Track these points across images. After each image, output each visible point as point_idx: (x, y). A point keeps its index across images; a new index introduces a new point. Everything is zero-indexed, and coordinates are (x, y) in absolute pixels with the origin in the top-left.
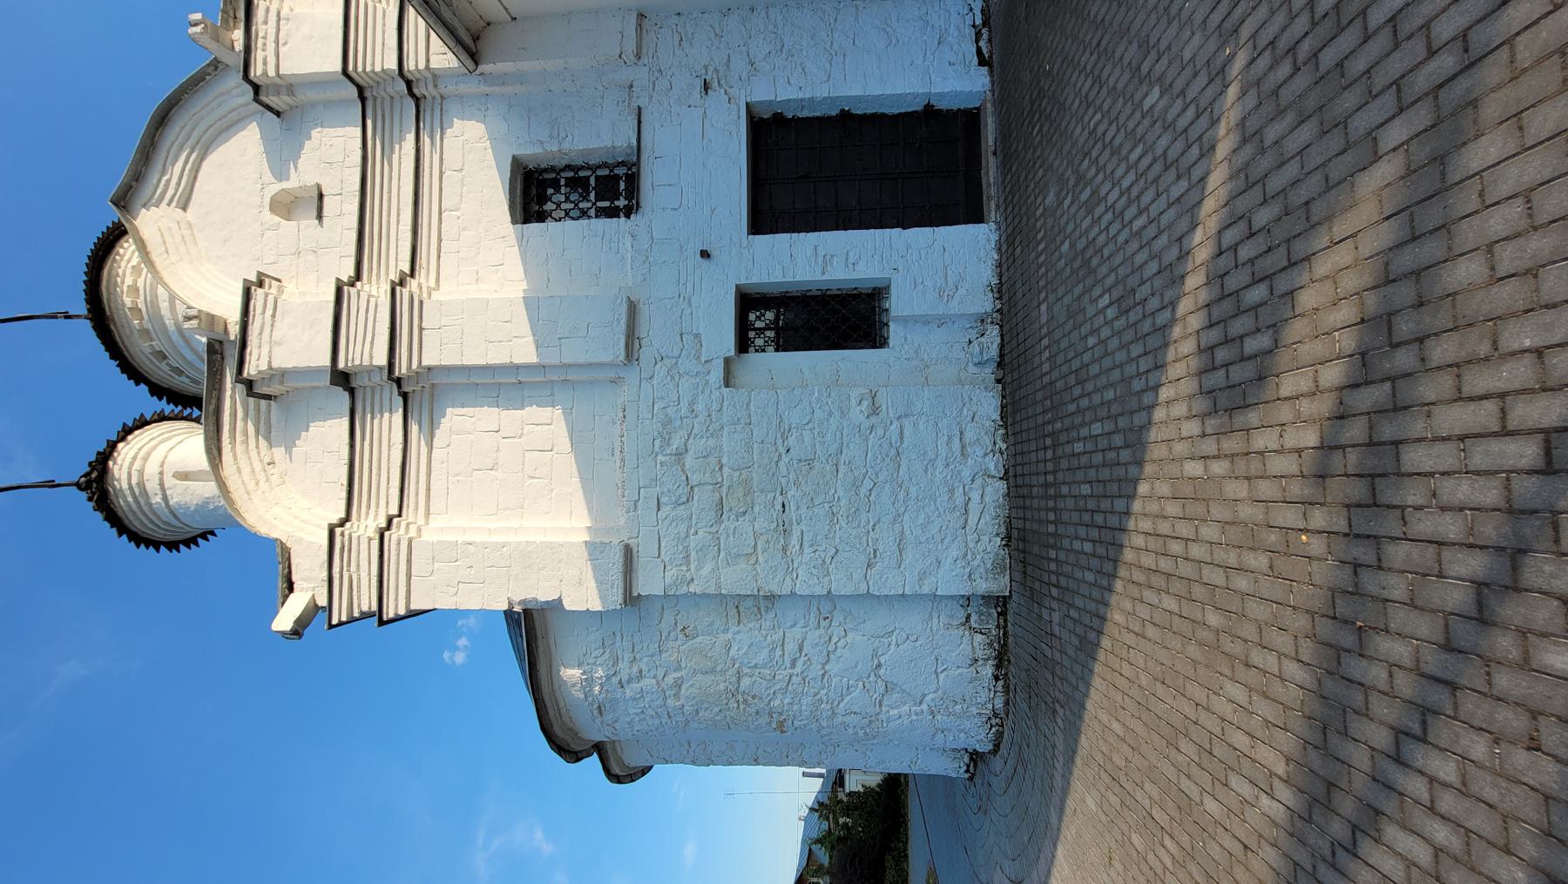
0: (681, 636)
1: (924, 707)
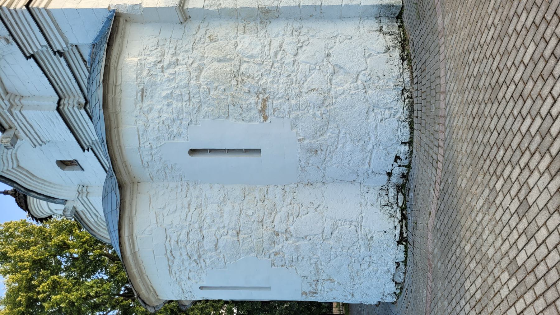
0: (207, 40)
1: (359, 82)
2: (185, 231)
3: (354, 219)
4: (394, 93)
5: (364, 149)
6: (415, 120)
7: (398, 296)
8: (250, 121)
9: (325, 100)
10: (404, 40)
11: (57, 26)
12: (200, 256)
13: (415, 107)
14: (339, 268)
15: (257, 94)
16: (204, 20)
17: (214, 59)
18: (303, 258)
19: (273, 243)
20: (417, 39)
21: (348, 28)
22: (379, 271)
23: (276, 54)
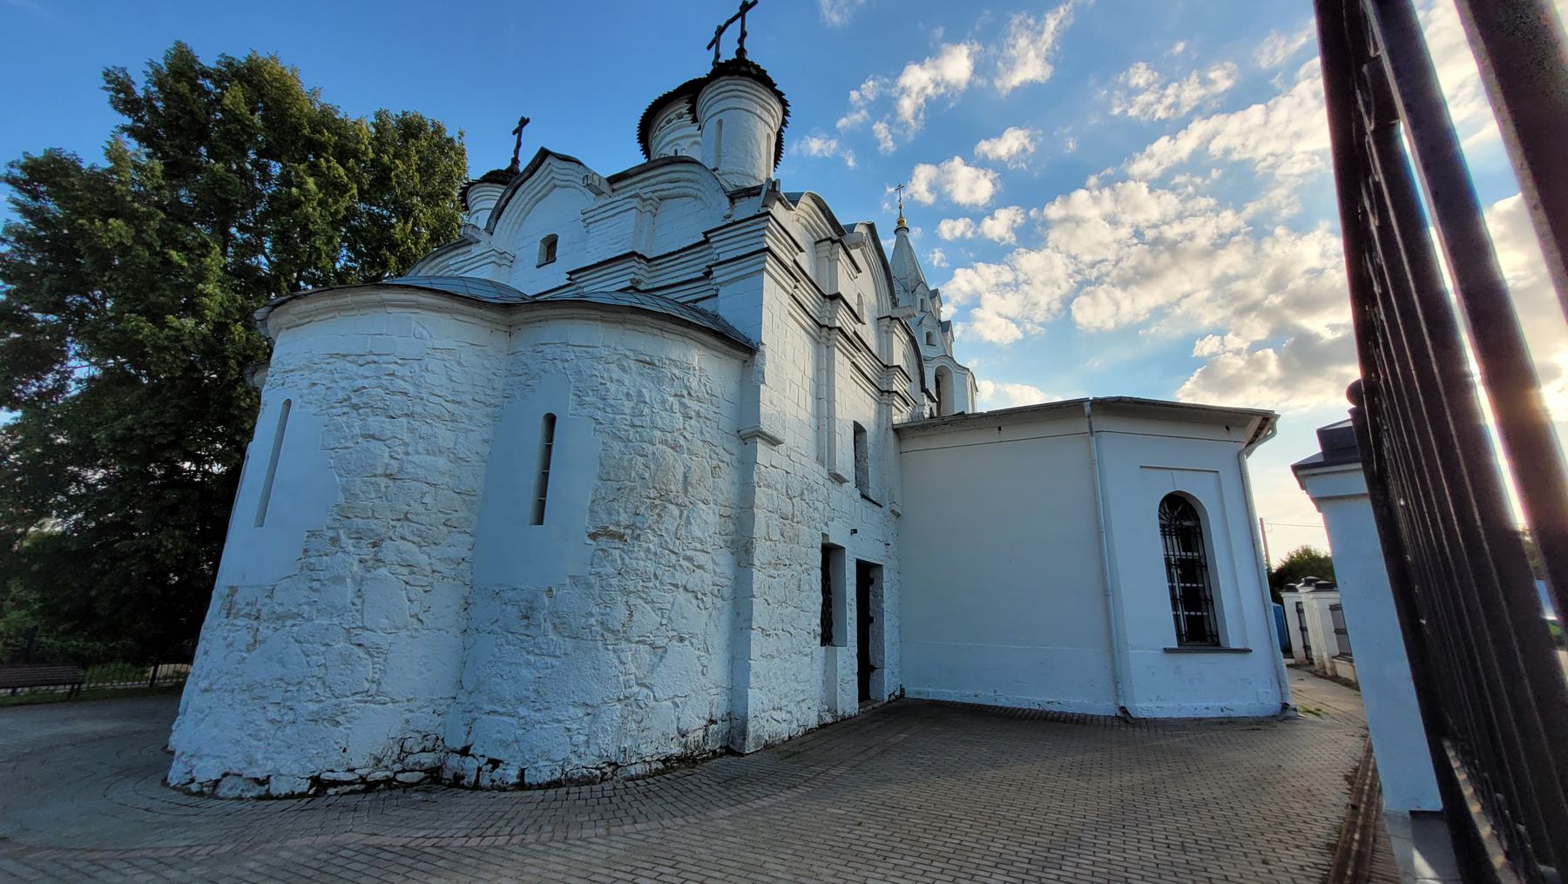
0: (714, 463)
1: (636, 689)
2: (410, 389)
3: (384, 688)
4: (613, 749)
5: (521, 701)
6: (562, 791)
7: (183, 789)
8: (591, 511)
9: (613, 632)
10: (695, 761)
11: (742, 277)
12: (356, 407)
13: (585, 788)
14: (280, 661)
15: (632, 526)
16: (741, 462)
17: (688, 468)
18: (316, 591)
19: (359, 536)
20: (695, 781)
21: (717, 670)
22: (254, 743)
23: (689, 559)
